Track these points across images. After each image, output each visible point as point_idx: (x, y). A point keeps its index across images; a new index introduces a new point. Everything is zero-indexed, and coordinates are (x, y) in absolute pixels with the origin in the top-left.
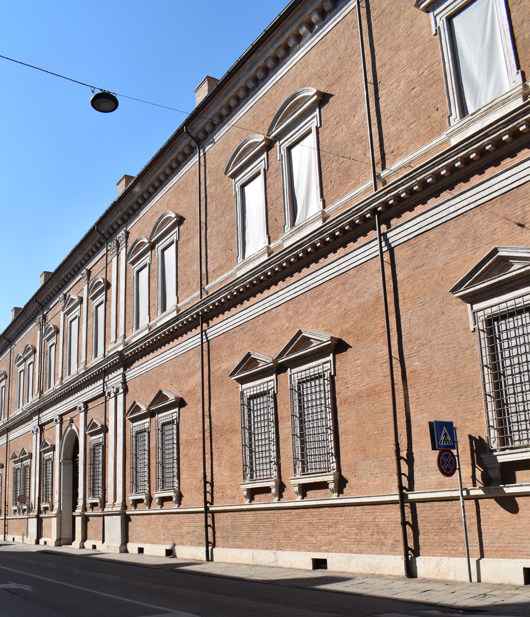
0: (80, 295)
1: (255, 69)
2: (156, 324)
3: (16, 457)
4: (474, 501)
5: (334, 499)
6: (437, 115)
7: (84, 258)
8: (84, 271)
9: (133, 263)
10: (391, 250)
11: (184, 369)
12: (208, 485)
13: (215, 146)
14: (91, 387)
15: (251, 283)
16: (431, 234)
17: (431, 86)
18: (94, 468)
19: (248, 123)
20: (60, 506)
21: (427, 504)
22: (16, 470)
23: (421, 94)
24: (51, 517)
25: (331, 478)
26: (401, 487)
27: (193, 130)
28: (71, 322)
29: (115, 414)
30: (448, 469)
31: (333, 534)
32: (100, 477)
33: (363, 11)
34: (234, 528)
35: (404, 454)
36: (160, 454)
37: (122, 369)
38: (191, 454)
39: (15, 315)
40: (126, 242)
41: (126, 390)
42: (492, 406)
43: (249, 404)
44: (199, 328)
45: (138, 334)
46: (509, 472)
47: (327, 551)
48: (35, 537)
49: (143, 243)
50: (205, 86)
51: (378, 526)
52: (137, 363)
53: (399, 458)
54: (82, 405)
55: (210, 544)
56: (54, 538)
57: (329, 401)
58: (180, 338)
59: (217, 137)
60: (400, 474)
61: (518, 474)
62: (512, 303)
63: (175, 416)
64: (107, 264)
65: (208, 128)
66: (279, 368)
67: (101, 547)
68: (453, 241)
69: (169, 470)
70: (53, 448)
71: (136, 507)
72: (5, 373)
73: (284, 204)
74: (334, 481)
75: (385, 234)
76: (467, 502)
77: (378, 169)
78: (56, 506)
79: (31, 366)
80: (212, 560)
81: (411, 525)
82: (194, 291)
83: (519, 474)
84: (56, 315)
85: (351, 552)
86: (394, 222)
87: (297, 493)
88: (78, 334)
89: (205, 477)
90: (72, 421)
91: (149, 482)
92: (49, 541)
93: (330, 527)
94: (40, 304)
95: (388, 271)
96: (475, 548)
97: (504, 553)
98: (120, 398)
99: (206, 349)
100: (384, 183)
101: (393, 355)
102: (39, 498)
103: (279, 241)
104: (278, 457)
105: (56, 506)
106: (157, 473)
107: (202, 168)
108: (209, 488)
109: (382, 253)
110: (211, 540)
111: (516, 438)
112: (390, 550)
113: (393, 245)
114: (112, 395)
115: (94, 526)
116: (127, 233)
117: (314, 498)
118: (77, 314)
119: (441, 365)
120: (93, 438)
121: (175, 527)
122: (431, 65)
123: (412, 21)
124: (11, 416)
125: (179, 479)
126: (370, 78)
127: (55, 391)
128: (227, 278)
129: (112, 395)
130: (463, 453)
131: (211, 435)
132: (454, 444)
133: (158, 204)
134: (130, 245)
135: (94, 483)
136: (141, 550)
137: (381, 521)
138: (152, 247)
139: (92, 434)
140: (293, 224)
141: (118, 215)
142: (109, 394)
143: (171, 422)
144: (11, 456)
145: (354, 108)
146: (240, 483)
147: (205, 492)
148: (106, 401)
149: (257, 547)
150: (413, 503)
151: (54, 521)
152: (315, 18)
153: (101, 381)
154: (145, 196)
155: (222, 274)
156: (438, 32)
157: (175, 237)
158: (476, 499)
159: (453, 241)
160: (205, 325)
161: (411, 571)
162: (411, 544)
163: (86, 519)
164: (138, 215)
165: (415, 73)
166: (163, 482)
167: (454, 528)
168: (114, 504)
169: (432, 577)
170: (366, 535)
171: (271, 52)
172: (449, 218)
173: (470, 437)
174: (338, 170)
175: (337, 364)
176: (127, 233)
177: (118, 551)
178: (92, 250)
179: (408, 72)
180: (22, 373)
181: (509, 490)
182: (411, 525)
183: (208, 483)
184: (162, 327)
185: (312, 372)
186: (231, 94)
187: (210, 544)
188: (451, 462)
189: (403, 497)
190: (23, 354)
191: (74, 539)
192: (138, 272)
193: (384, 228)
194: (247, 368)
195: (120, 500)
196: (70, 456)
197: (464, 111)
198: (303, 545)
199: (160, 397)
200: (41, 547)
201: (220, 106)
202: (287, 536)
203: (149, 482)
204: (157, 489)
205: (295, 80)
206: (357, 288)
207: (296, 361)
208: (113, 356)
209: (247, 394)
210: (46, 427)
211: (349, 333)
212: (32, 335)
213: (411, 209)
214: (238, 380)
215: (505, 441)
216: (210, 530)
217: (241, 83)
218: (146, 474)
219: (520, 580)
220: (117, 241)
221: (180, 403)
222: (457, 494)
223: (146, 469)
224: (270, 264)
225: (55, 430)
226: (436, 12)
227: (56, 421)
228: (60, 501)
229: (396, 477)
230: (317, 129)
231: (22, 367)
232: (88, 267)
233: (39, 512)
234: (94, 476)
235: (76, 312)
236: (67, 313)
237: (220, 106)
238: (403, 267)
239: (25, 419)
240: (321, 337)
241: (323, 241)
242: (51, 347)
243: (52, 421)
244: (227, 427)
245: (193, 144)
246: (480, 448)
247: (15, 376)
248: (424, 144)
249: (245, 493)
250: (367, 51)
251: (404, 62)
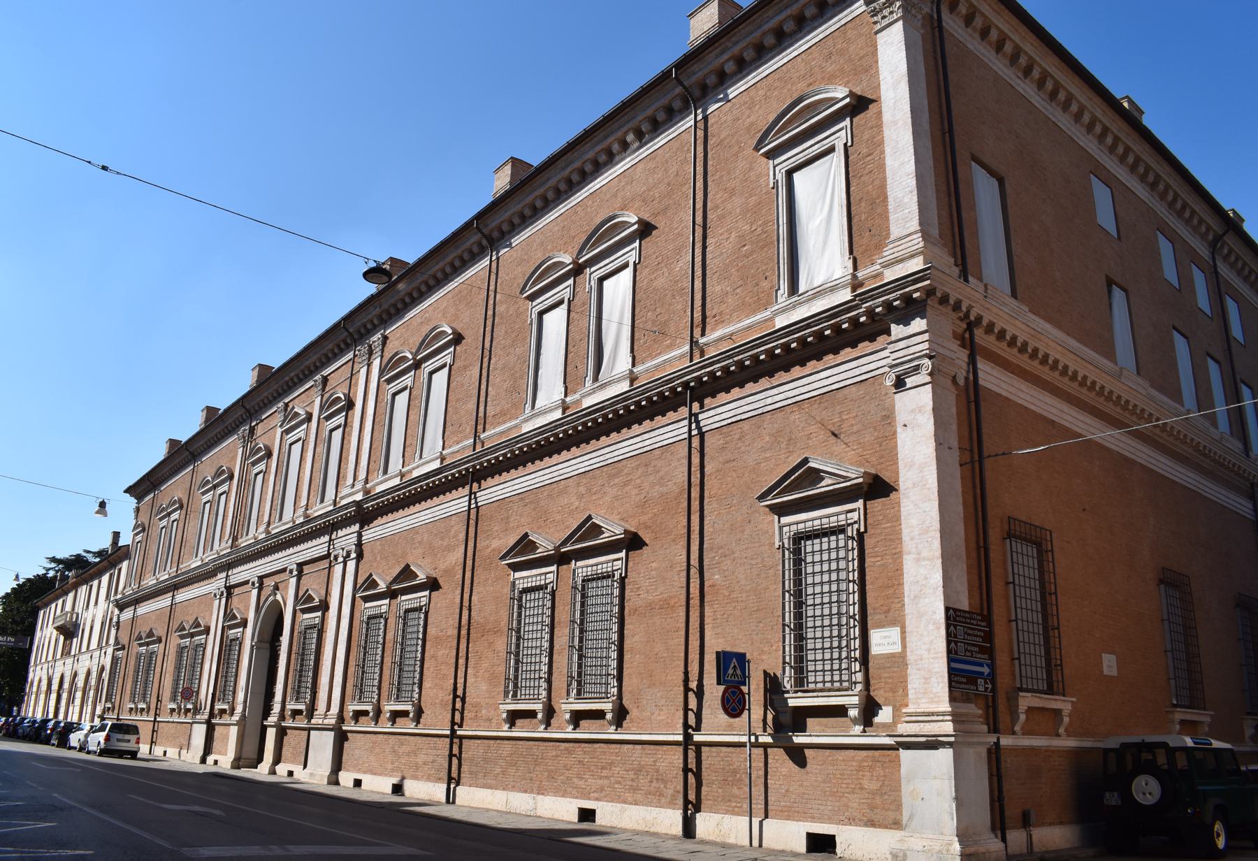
0: (308, 409)
1: (569, 169)
2: (410, 471)
3: (184, 629)
4: (951, 751)
5: (855, 735)
6: (765, 284)
7: (320, 360)
8: (318, 377)
9: (389, 381)
10: (702, 435)
11: (442, 539)
12: (458, 700)
13: (512, 252)
14: (310, 544)
15: (538, 442)
16: (746, 425)
17: (762, 248)
18: (302, 660)
19: (549, 235)
20: (244, 710)
21: (714, 749)
22: (181, 650)
23: (751, 254)
24: (229, 725)
25: (855, 700)
26: (686, 726)
27: (486, 226)
28: (291, 444)
29: (341, 587)
30: (734, 709)
31: (607, 777)
32: (311, 674)
33: (700, 133)
34: (486, 760)
35: (693, 685)
36: (398, 651)
37: (358, 525)
38: (440, 657)
39: (206, 421)
40: (382, 351)
41: (360, 556)
42: (790, 639)
43: (520, 600)
44: (468, 487)
45: (386, 480)
46: (800, 718)
47: (597, 799)
48: (201, 753)
49: (404, 359)
50: (508, 170)
51: (657, 771)
52: (380, 521)
53: (687, 689)
54: (295, 566)
55: (453, 780)
56: (231, 755)
57: (616, 609)
58: (441, 497)
59: (516, 241)
60: (686, 709)
61: (810, 721)
62: (817, 522)
63: (424, 601)
65: (505, 227)
66: (561, 559)
67: (300, 774)
68: (767, 439)
69: (408, 676)
70: (244, 624)
71: (357, 721)
72: (180, 501)
73: (587, 353)
74: (612, 711)
75: (696, 415)
76: (755, 751)
77: (697, 332)
78: (239, 709)
79: (223, 497)
80: (454, 802)
81: (693, 772)
82: (466, 438)
83: (810, 722)
84: (270, 429)
85: (625, 802)
86: (707, 401)
87: (568, 722)
88: (300, 466)
89: (455, 689)
90: (276, 588)
91: (379, 688)
92: (223, 760)
93: (603, 768)
94: (248, 411)
95: (696, 460)
96: (759, 806)
97: (789, 814)
98: (351, 565)
99: (473, 517)
100: (702, 354)
101: (692, 562)
102: (214, 695)
103: (577, 396)
104: (550, 672)
105: (239, 709)
106: (391, 676)
107: (493, 277)
108: (459, 705)
109: (690, 436)
110: (454, 775)
111: (811, 679)
112: (670, 803)
113: (704, 429)
114: (340, 559)
115: (293, 743)
116: (385, 338)
117: (588, 731)
118: (302, 435)
119: (743, 582)
120: (306, 616)
121: (408, 754)
122: (765, 223)
123: (751, 164)
124: (184, 567)
125: (420, 687)
126: (699, 219)
127: (257, 542)
128: (510, 429)
129: (340, 559)
130: (755, 691)
131: (469, 634)
132: (744, 679)
133: (431, 309)
134: (387, 355)
135: (300, 682)
136: (358, 783)
137: (662, 765)
138: (417, 365)
139: (304, 611)
140: (596, 379)
141: (374, 312)
142: (336, 558)
143: (419, 609)
144: (175, 627)
145: (678, 251)
147: (454, 710)
148: (330, 566)
149: (513, 789)
150: (699, 746)
151: (234, 731)
152: (645, 127)
153: (327, 538)
154: (415, 295)
155: (504, 422)
156: (776, 186)
157: (566, 294)
158: (765, 746)
159: (767, 439)
160: (475, 485)
161: (689, 830)
162: (692, 797)
163: (282, 733)
164: (402, 317)
165: (747, 227)
166: (399, 690)
167: (740, 780)
168: (326, 714)
169: (711, 838)
170: (643, 781)
171: (591, 154)
172: (744, 417)
173: (765, 672)
174: (654, 322)
175: (630, 564)
176: (385, 338)
177: (325, 781)
178: (332, 351)
179: (740, 224)
180: (208, 506)
181: (799, 739)
182: (693, 772)
183: (458, 697)
184: (383, 494)
185: (600, 569)
186: (537, 193)
187: (453, 780)
188: (739, 701)
189: (687, 737)
190: (213, 479)
191: (260, 759)
192: (394, 395)
193: (696, 406)
194: (523, 553)
195: (335, 709)
196: (268, 637)
197: (793, 288)
198: (569, 789)
199: (407, 573)
200: (209, 767)
201: (522, 204)
202: (551, 777)
203: (379, 688)
204: (389, 699)
205: (615, 196)
206: (661, 474)
208: (347, 506)
209: (521, 585)
210: (237, 591)
211: (647, 527)
212: (230, 452)
213: (836, 352)
214: (509, 565)
215: (800, 682)
216: (455, 761)
217: (552, 183)
218: (377, 676)
219: (801, 846)
220: (370, 346)
221: (433, 585)
222: (744, 739)
223: (377, 670)
224: (562, 425)
226: (777, 161)
227: (253, 584)
228: (245, 702)
229: (681, 713)
230: (635, 264)
231: (208, 497)
232: (325, 372)
233: (212, 715)
234: (301, 671)
235: (299, 432)
236: (288, 432)
237: (522, 204)
238: (712, 459)
239: (206, 574)
240: (613, 530)
241: (626, 408)
242: (257, 474)
243: (246, 582)
244: (490, 626)
245: (485, 242)
246: (773, 687)
247: (154, 532)
248: (748, 316)
249: (504, 715)
250: (700, 184)
251: (738, 211)
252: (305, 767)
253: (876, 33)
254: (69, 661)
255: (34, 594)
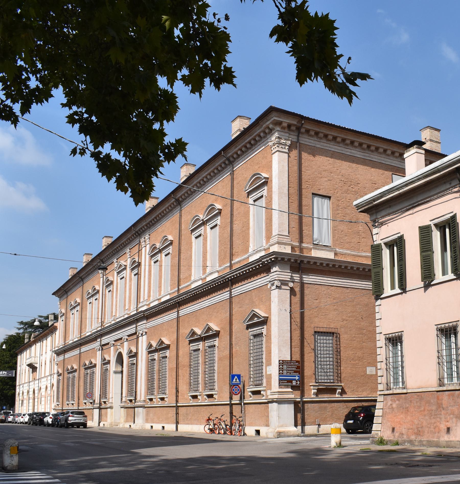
27: (177, 196)
64: (139, 251)
146: (311, 384)
153: (135, 326)
186: (264, 126)
225: (110, 350)
252: (134, 423)
253: (272, 154)
254: (37, 382)
255: (16, 345)
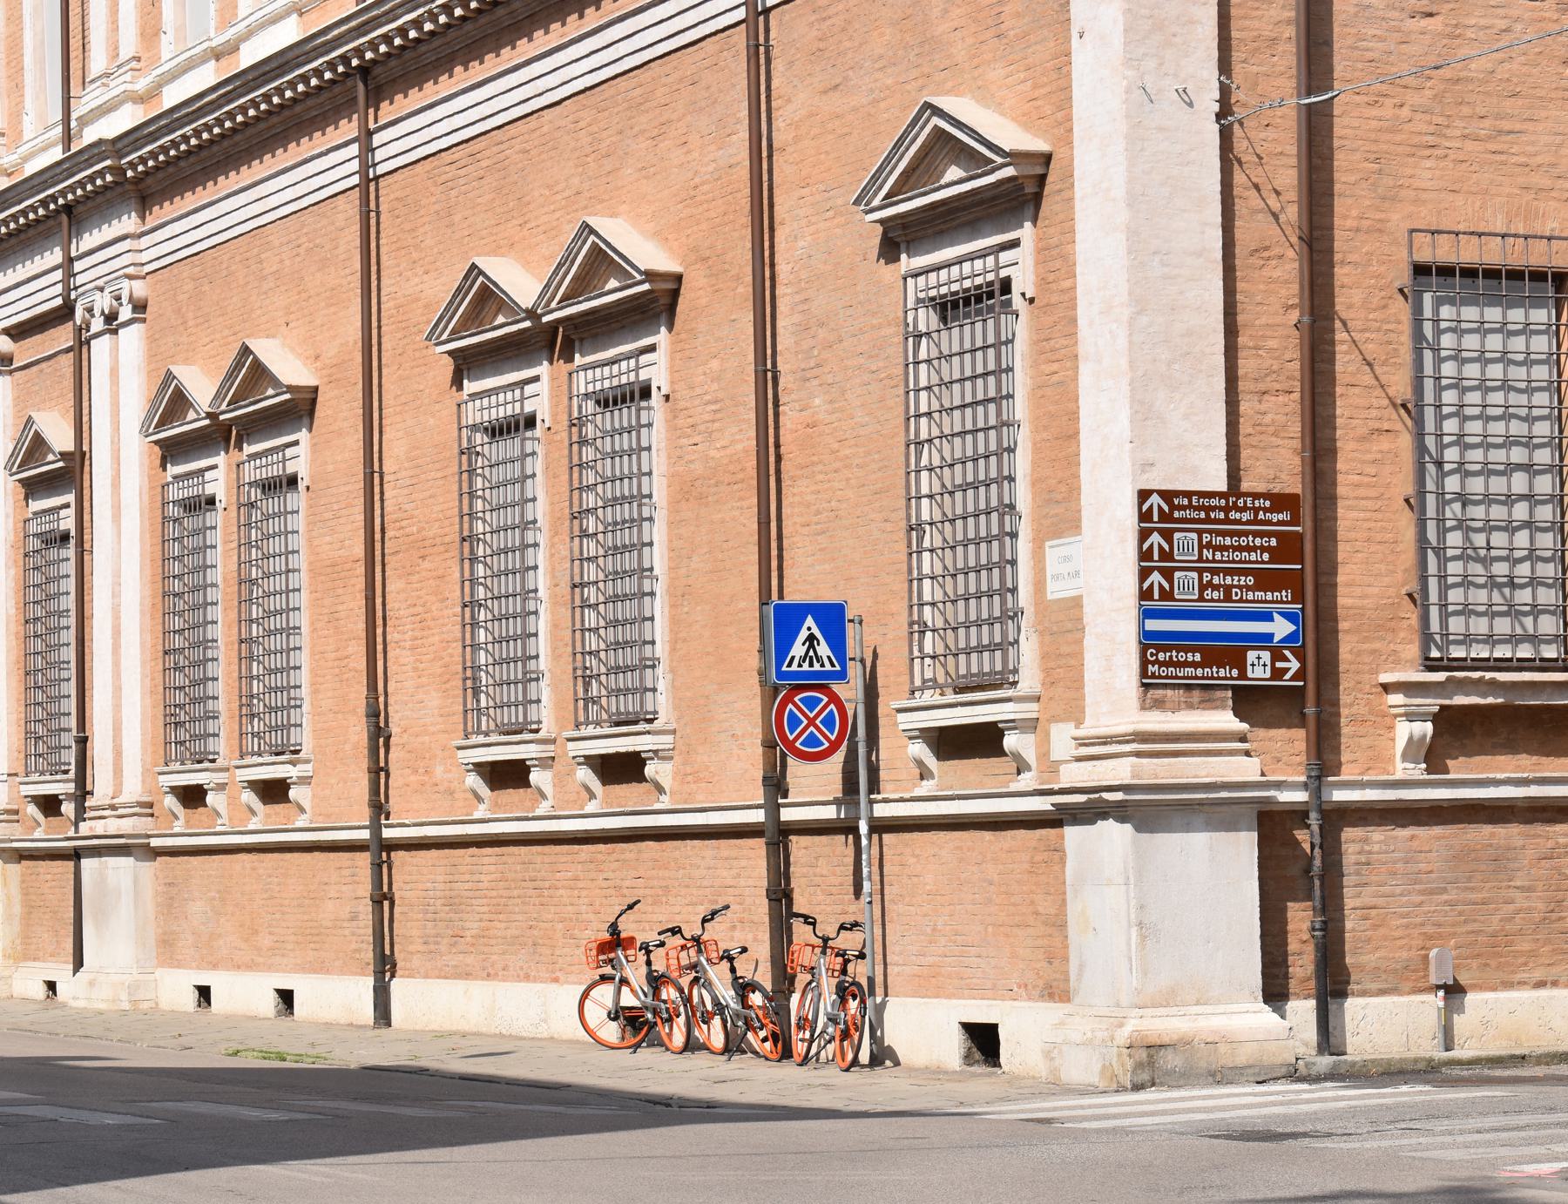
34: (452, 903)
146: (1386, 678)
153: (55, 256)
161: (383, 1012)
207: (588, 323)
252: (78, 963)
